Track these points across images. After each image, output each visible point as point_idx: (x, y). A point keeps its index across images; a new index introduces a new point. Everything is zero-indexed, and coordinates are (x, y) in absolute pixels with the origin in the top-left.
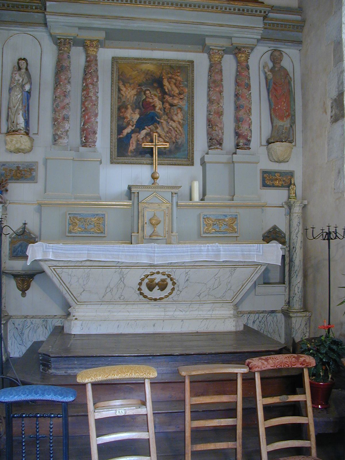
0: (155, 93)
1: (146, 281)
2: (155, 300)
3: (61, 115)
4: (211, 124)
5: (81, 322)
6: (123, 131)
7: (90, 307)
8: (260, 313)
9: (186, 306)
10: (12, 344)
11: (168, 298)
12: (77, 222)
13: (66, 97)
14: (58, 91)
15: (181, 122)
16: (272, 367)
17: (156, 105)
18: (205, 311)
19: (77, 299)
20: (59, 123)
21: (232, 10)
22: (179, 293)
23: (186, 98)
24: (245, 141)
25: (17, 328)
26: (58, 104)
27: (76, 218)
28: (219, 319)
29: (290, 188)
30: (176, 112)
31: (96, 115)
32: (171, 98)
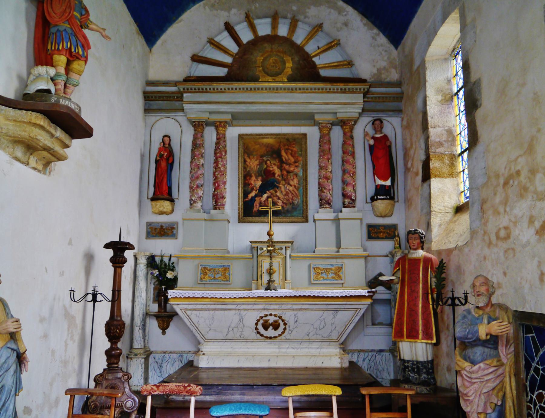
0: (274, 162)
1: (261, 321)
2: (271, 338)
3: (195, 184)
4: (321, 187)
5: (207, 357)
6: (248, 195)
7: (216, 343)
8: (369, 352)
9: (298, 344)
10: (152, 376)
11: (281, 337)
12: (208, 272)
13: (199, 169)
14: (193, 164)
15: (297, 185)
16: (162, 392)
17: (275, 173)
18: (314, 349)
19: (205, 337)
20: (193, 190)
21: (336, 90)
22: (290, 332)
23: (300, 165)
24: (349, 200)
25: (157, 362)
26: (193, 175)
27: (206, 268)
28: (326, 356)
29: (395, 239)
30: (292, 178)
31: (225, 183)
32: (288, 166)
